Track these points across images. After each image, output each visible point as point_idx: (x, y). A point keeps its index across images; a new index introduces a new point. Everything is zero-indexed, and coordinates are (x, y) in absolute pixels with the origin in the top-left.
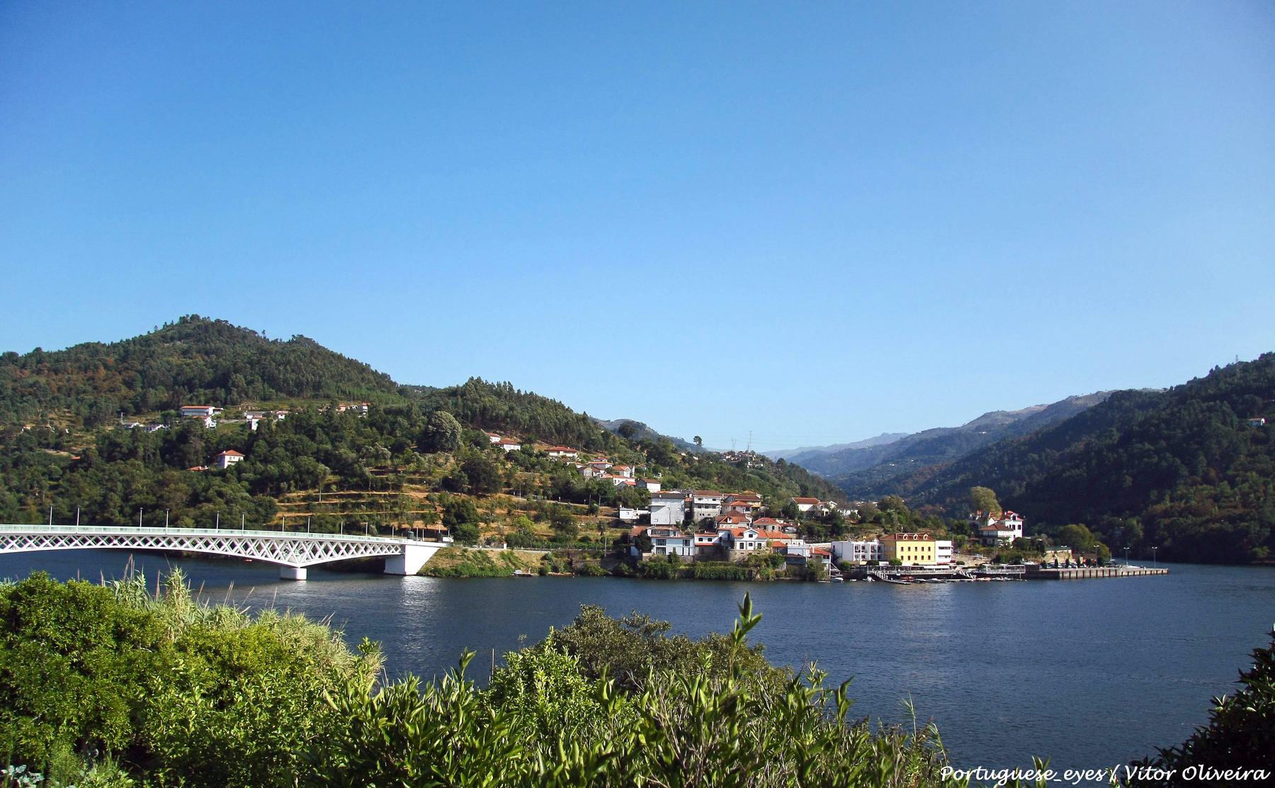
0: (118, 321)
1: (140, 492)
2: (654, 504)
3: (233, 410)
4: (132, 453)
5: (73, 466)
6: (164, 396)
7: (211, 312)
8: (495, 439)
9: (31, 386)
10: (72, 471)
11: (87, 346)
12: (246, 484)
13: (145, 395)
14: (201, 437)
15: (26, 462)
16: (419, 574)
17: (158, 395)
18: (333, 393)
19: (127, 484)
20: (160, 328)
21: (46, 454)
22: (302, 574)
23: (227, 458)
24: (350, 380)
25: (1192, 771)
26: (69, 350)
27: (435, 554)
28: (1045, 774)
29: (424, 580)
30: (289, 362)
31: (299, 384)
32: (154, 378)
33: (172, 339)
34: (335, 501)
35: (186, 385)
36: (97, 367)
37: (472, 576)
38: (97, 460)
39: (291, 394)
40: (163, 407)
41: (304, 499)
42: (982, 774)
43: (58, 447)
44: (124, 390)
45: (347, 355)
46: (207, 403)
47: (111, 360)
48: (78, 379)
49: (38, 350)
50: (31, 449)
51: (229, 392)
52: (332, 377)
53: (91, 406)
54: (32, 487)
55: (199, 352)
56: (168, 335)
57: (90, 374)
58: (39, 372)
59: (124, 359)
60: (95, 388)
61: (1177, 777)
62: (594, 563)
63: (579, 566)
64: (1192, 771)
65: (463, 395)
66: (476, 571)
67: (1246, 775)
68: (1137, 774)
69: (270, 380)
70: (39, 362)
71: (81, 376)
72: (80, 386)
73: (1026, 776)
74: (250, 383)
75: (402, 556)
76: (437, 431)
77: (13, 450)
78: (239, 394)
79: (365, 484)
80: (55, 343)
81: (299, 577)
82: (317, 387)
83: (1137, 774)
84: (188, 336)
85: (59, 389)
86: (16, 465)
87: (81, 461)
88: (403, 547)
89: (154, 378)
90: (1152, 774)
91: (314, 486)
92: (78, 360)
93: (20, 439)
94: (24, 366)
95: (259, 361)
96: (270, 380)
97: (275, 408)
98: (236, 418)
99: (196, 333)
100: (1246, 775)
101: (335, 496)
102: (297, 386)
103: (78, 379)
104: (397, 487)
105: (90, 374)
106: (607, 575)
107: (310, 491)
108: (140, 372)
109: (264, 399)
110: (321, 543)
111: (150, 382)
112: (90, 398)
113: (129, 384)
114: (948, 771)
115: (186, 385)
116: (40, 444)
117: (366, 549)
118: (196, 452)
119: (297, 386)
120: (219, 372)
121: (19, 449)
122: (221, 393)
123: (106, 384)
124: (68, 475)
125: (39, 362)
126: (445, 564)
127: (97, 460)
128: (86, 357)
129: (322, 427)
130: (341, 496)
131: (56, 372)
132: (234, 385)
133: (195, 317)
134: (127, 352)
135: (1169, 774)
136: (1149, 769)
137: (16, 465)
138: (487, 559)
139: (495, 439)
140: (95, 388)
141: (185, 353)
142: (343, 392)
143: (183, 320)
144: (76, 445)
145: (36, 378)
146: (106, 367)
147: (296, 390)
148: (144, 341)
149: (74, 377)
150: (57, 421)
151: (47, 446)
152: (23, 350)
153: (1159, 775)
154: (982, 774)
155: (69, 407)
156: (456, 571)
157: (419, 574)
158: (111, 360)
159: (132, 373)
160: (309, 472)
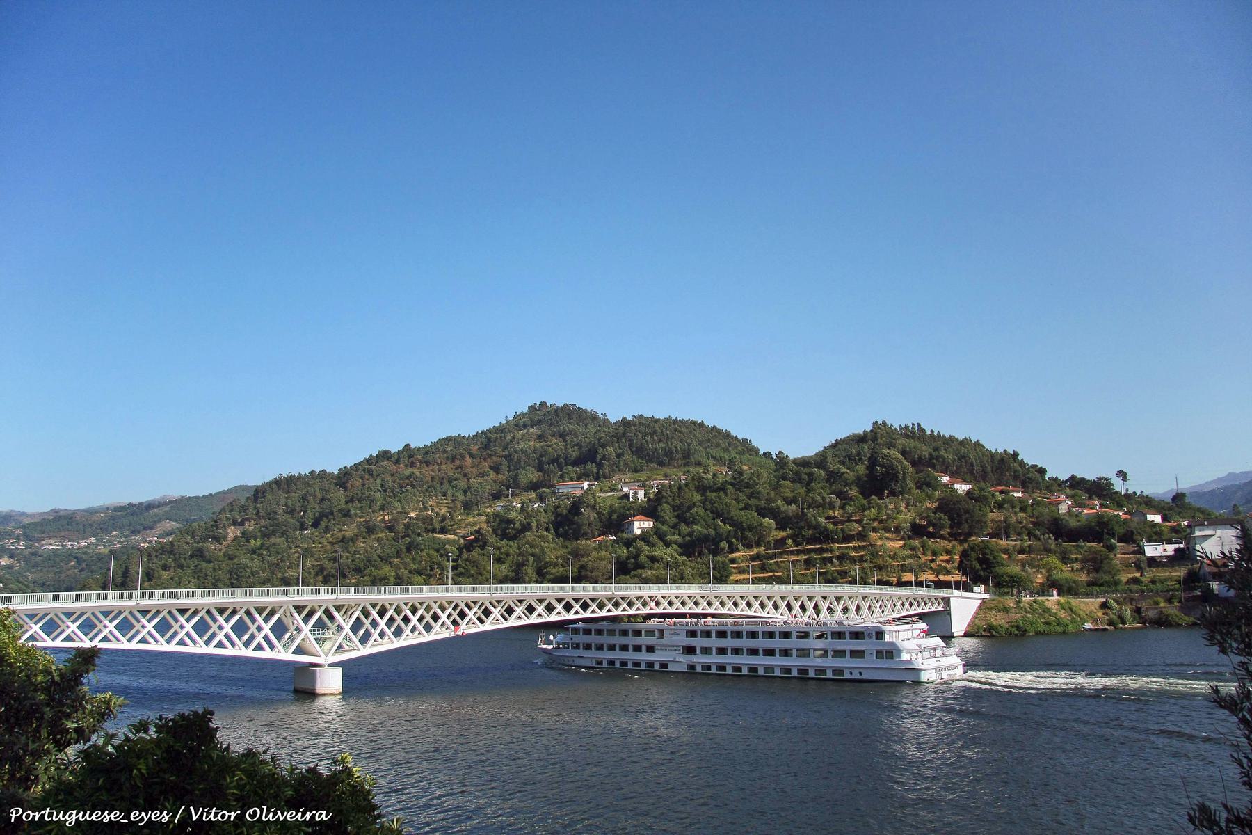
0: (475, 415)
1: (555, 565)
2: (1198, 533)
3: (607, 484)
4: (526, 527)
5: (469, 546)
6: (535, 476)
7: (557, 399)
8: (945, 479)
9: (408, 478)
10: (469, 551)
11: (449, 439)
12: (675, 547)
13: (516, 476)
14: (593, 507)
15: (417, 547)
16: (966, 635)
17: (529, 475)
18: (703, 460)
19: (538, 558)
20: (511, 418)
21: (434, 538)
22: (330, 681)
23: (636, 524)
24: (718, 445)
25: (255, 812)
26: (434, 444)
27: (980, 608)
28: (112, 815)
29: (969, 640)
30: (655, 432)
31: (668, 453)
32: (519, 461)
33: (525, 426)
34: (793, 558)
35: (551, 466)
36: (463, 457)
37: (1038, 634)
38: (491, 539)
39: (661, 464)
40: (534, 486)
41: (753, 558)
42: (50, 815)
43: (443, 531)
44: (492, 475)
45: (709, 423)
46: (579, 479)
47: (475, 449)
48: (448, 469)
49: (408, 446)
50: (419, 535)
51: (600, 466)
52: (700, 443)
53: (465, 492)
54: (432, 569)
55: (553, 435)
56: (519, 423)
57: (457, 463)
58: (412, 465)
59: (486, 447)
60: (465, 475)
61: (240, 818)
62: (1173, 610)
63: (1152, 614)
64: (255, 812)
65: (874, 439)
66: (1041, 628)
67: (308, 816)
68: (201, 815)
69: (639, 451)
70: (410, 456)
71: (449, 466)
72: (451, 474)
73: (94, 817)
74: (619, 456)
75: (947, 612)
76: (888, 473)
77: (403, 537)
78: (610, 466)
79: (823, 536)
80: (421, 439)
81: (320, 687)
82: (687, 455)
83: (201, 815)
84: (539, 422)
85: (432, 478)
86: (409, 550)
87: (476, 540)
88: (947, 601)
89: (519, 461)
90: (216, 815)
91: (758, 545)
92: (445, 451)
93: (407, 526)
94: (397, 462)
95: (624, 435)
96: (639, 451)
97: (649, 478)
98: (612, 490)
99: (544, 418)
100: (308, 816)
101: (792, 552)
102: (666, 455)
103: (448, 469)
104: (862, 536)
105: (457, 463)
106: (1194, 624)
107: (755, 550)
108: (505, 457)
109: (636, 471)
110: (838, 599)
111: (515, 466)
112: (462, 484)
113: (496, 469)
114: (17, 811)
115: (551, 466)
116: (427, 530)
117: (911, 605)
118: (590, 524)
119: (666, 455)
120: (584, 449)
121: (408, 536)
122: (592, 467)
123: (474, 470)
124: (465, 555)
125: (410, 456)
126: (999, 620)
127: (491, 539)
128: (451, 448)
129: (731, 484)
130: (799, 552)
131: (427, 463)
132: (604, 458)
133: (543, 404)
134: (489, 440)
135: (233, 815)
136: (214, 810)
137: (409, 550)
138: (1046, 610)
139: (945, 479)
140: (465, 475)
141: (540, 438)
142: (714, 458)
143: (532, 408)
144: (460, 528)
145: (410, 471)
146: (471, 455)
147: (663, 460)
148: (501, 429)
149: (443, 467)
150: (437, 507)
151: (434, 531)
152: (394, 448)
153: (223, 816)
154: (50, 815)
155: (445, 494)
156: (1018, 627)
157: (966, 635)
158: (475, 449)
159: (499, 459)
160: (750, 528)
